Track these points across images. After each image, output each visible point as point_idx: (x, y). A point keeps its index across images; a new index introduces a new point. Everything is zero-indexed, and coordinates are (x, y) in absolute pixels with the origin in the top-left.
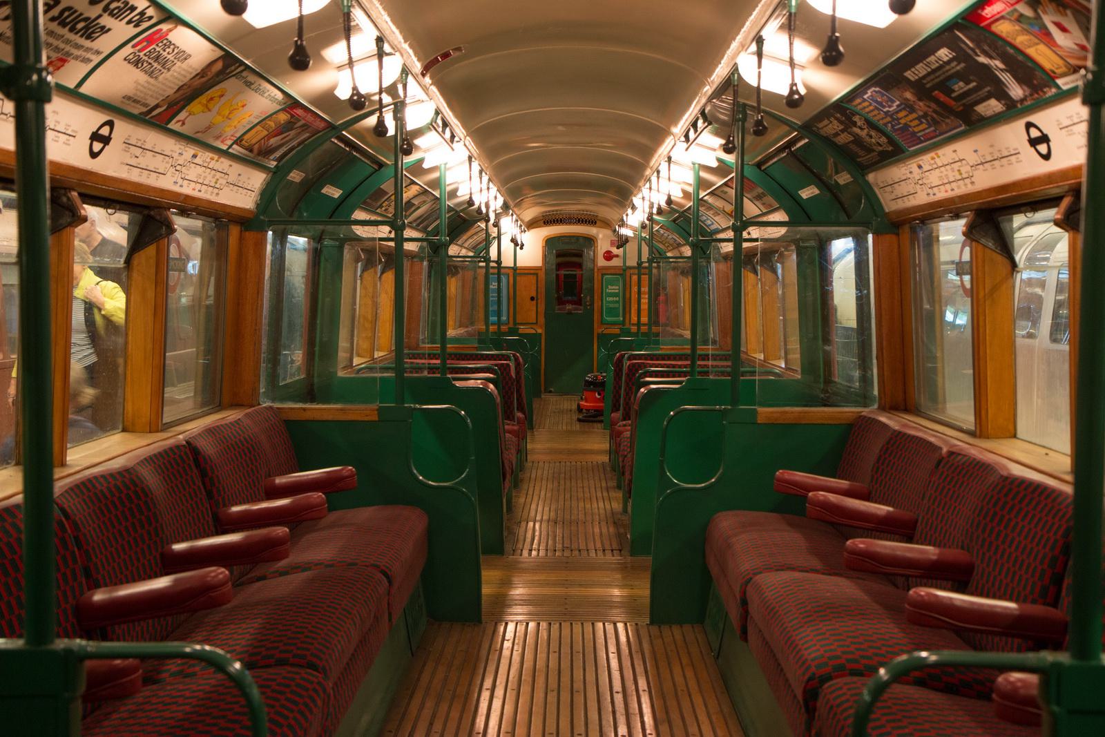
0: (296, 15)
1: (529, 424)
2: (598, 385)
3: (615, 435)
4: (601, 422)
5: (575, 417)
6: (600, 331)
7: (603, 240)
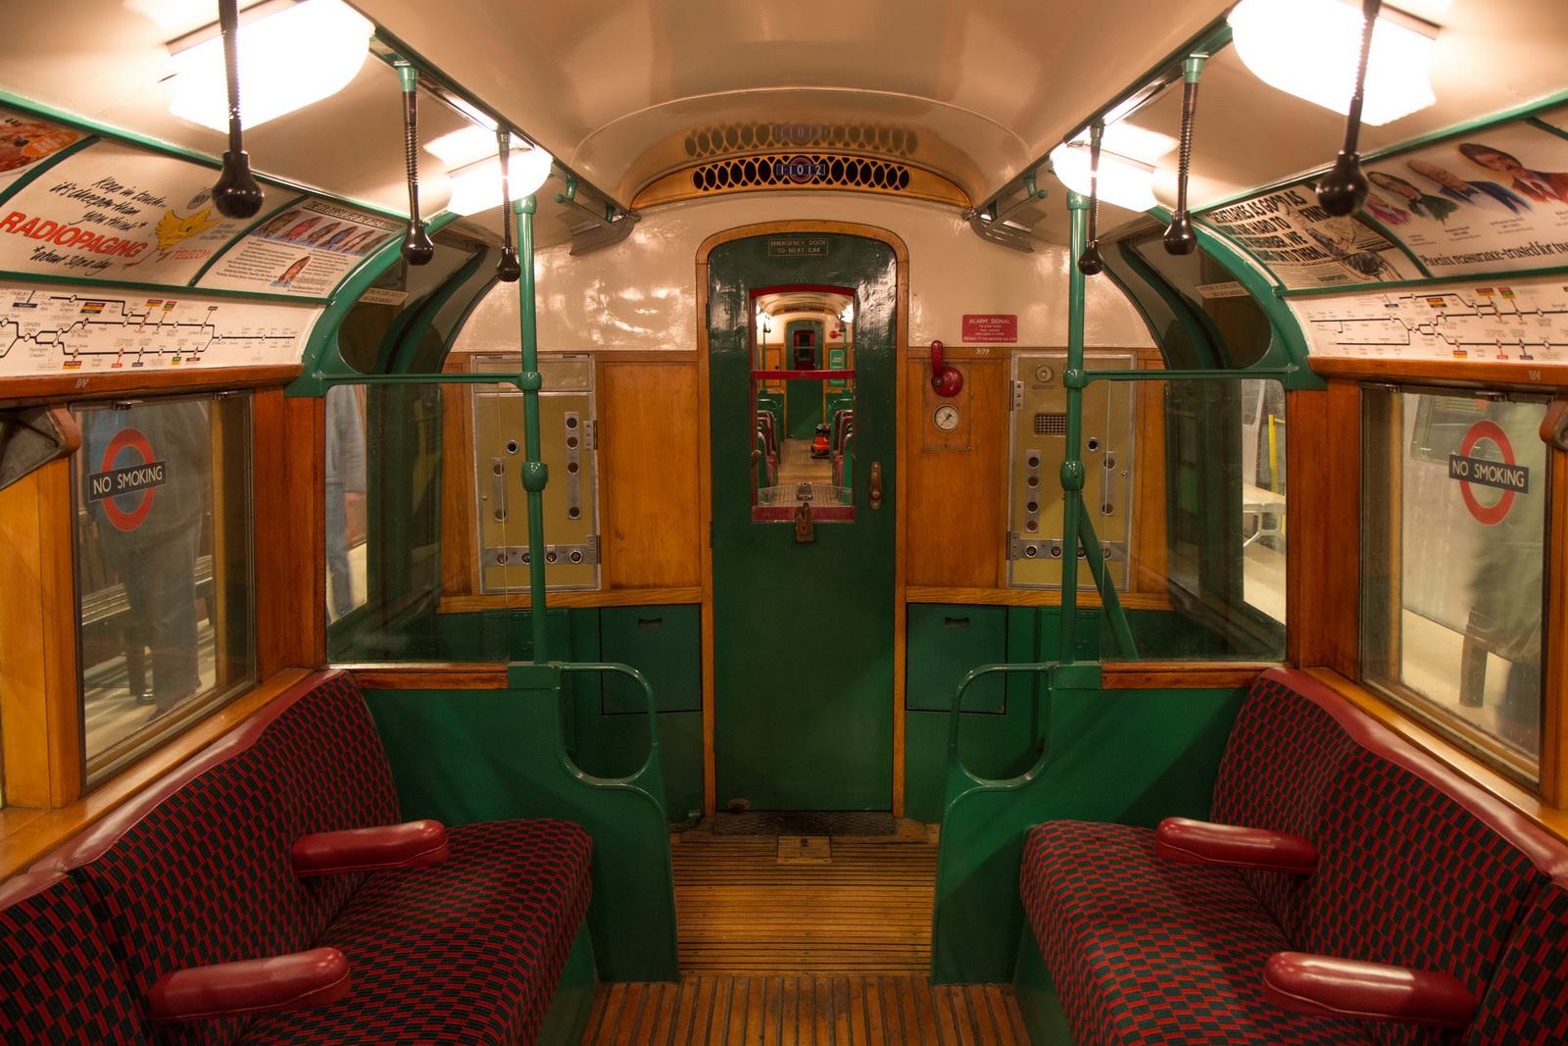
0: (498, 202)
1: (778, 462)
2: (825, 432)
3: (835, 465)
4: (828, 458)
5: (810, 455)
6: (829, 391)
7: (830, 323)
